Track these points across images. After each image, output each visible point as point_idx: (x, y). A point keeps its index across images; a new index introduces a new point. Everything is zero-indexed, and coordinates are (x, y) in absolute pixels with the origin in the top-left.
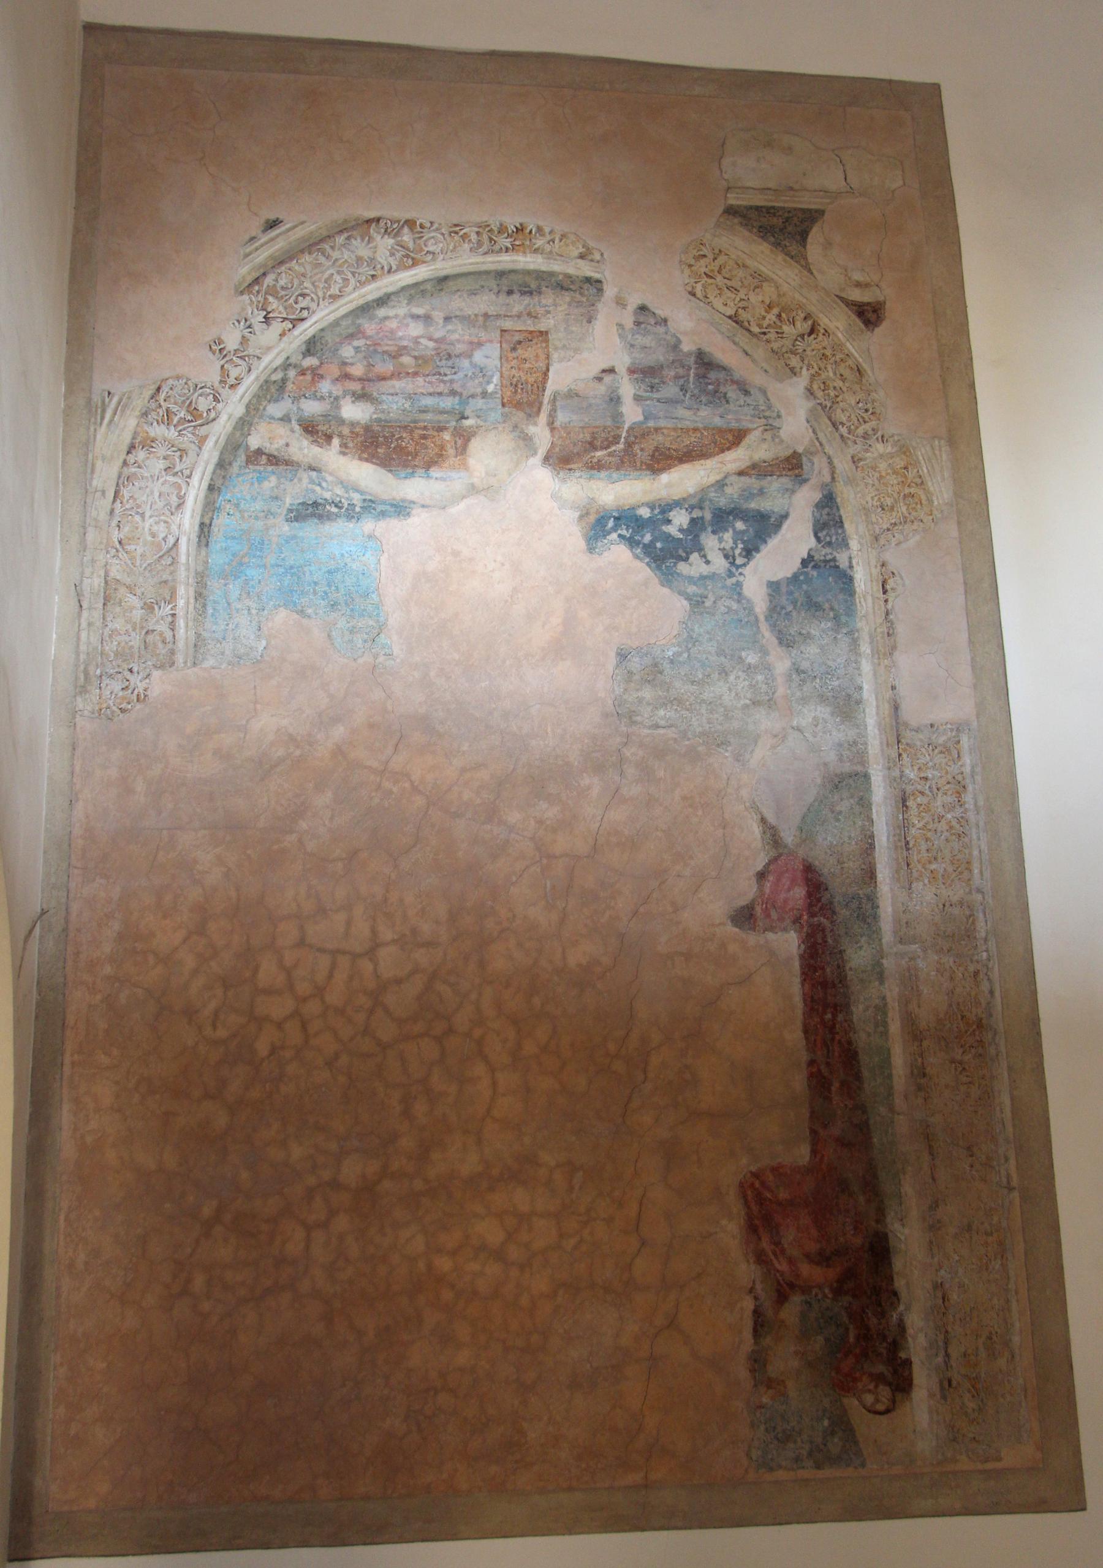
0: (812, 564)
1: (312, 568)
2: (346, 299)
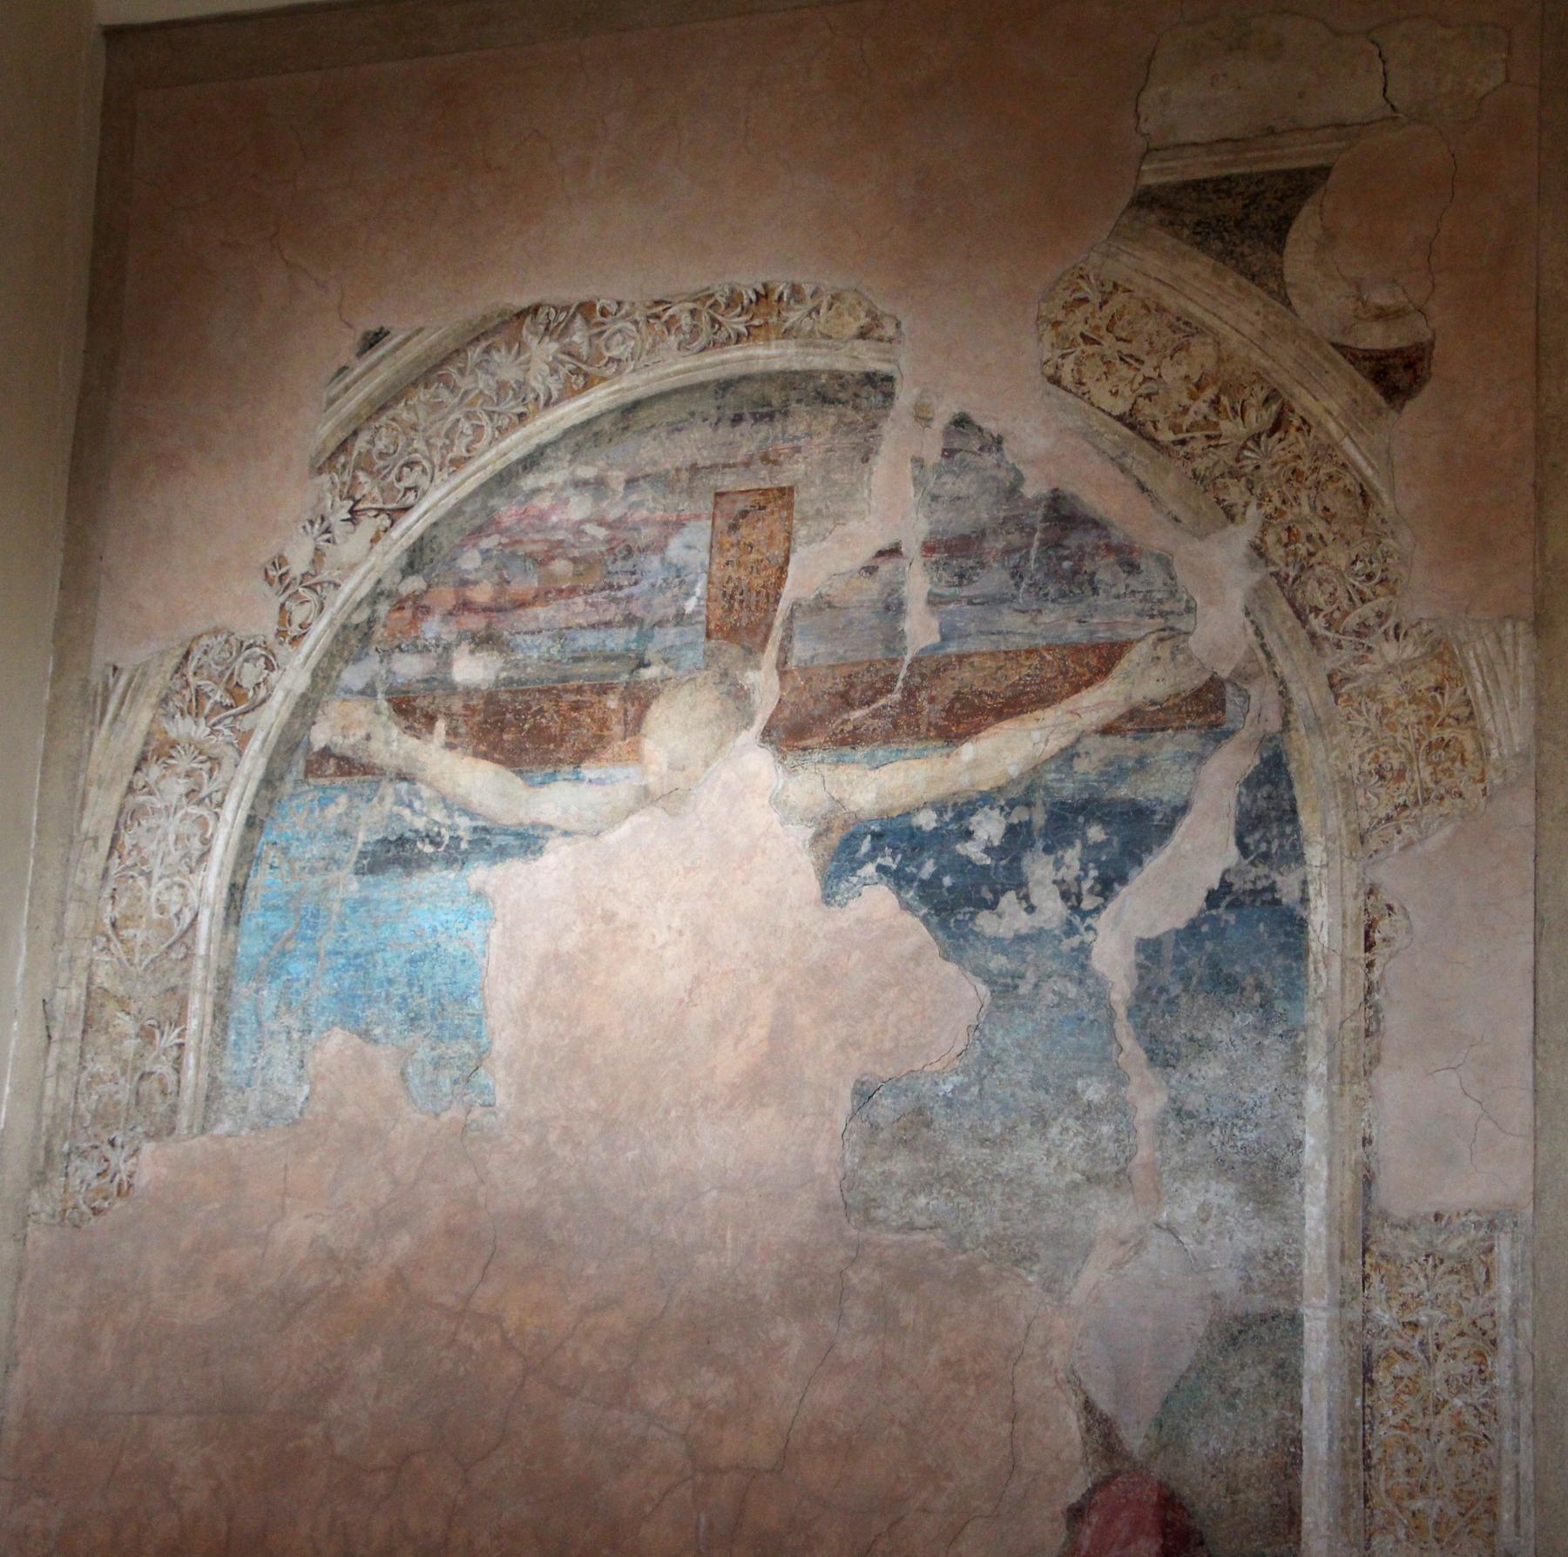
0: (1228, 898)
1: (388, 955)
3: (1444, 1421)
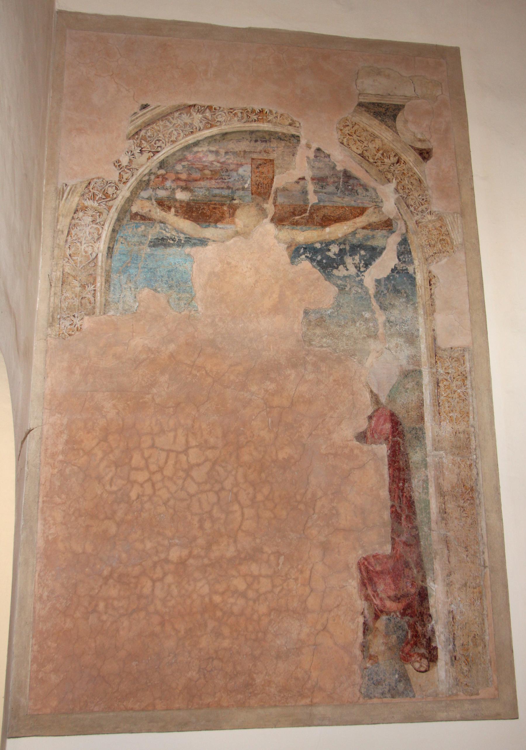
1: (161, 269)
3: (456, 396)
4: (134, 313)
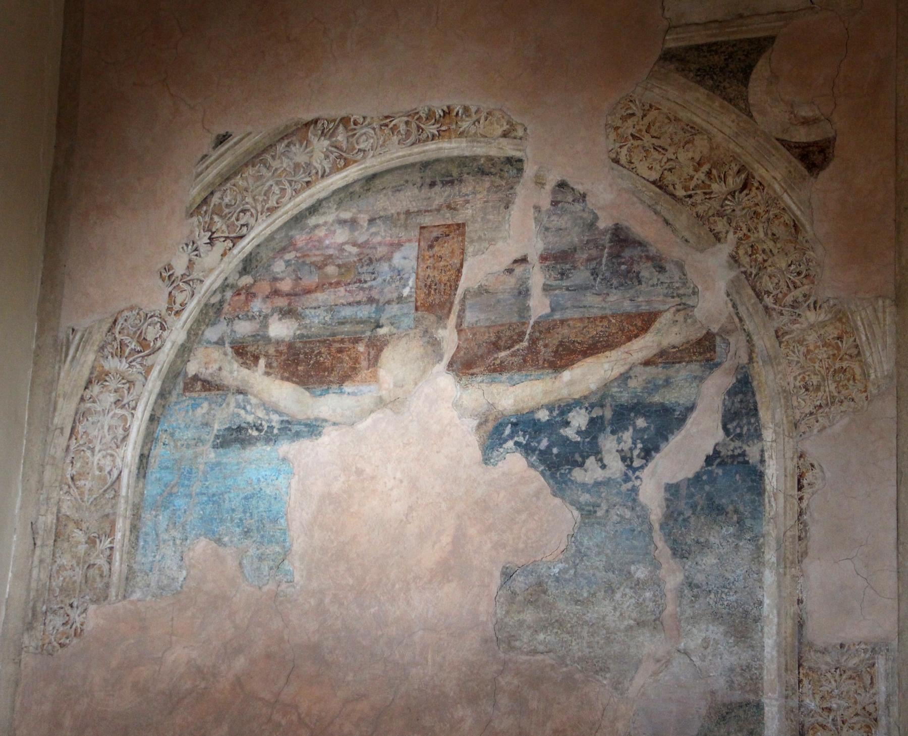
0: (718, 460)
1: (232, 495)
2: (283, 210)
4: (178, 593)
